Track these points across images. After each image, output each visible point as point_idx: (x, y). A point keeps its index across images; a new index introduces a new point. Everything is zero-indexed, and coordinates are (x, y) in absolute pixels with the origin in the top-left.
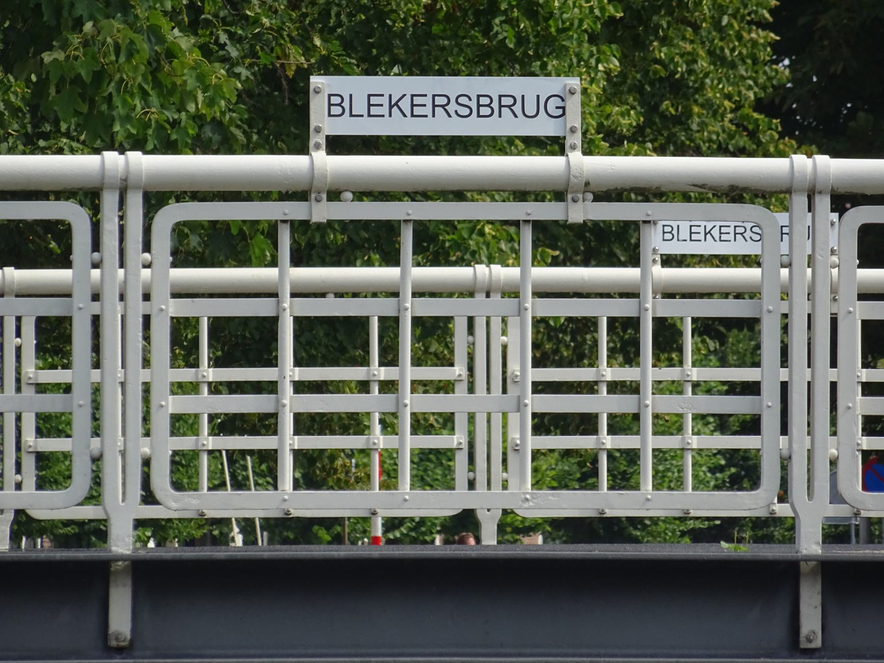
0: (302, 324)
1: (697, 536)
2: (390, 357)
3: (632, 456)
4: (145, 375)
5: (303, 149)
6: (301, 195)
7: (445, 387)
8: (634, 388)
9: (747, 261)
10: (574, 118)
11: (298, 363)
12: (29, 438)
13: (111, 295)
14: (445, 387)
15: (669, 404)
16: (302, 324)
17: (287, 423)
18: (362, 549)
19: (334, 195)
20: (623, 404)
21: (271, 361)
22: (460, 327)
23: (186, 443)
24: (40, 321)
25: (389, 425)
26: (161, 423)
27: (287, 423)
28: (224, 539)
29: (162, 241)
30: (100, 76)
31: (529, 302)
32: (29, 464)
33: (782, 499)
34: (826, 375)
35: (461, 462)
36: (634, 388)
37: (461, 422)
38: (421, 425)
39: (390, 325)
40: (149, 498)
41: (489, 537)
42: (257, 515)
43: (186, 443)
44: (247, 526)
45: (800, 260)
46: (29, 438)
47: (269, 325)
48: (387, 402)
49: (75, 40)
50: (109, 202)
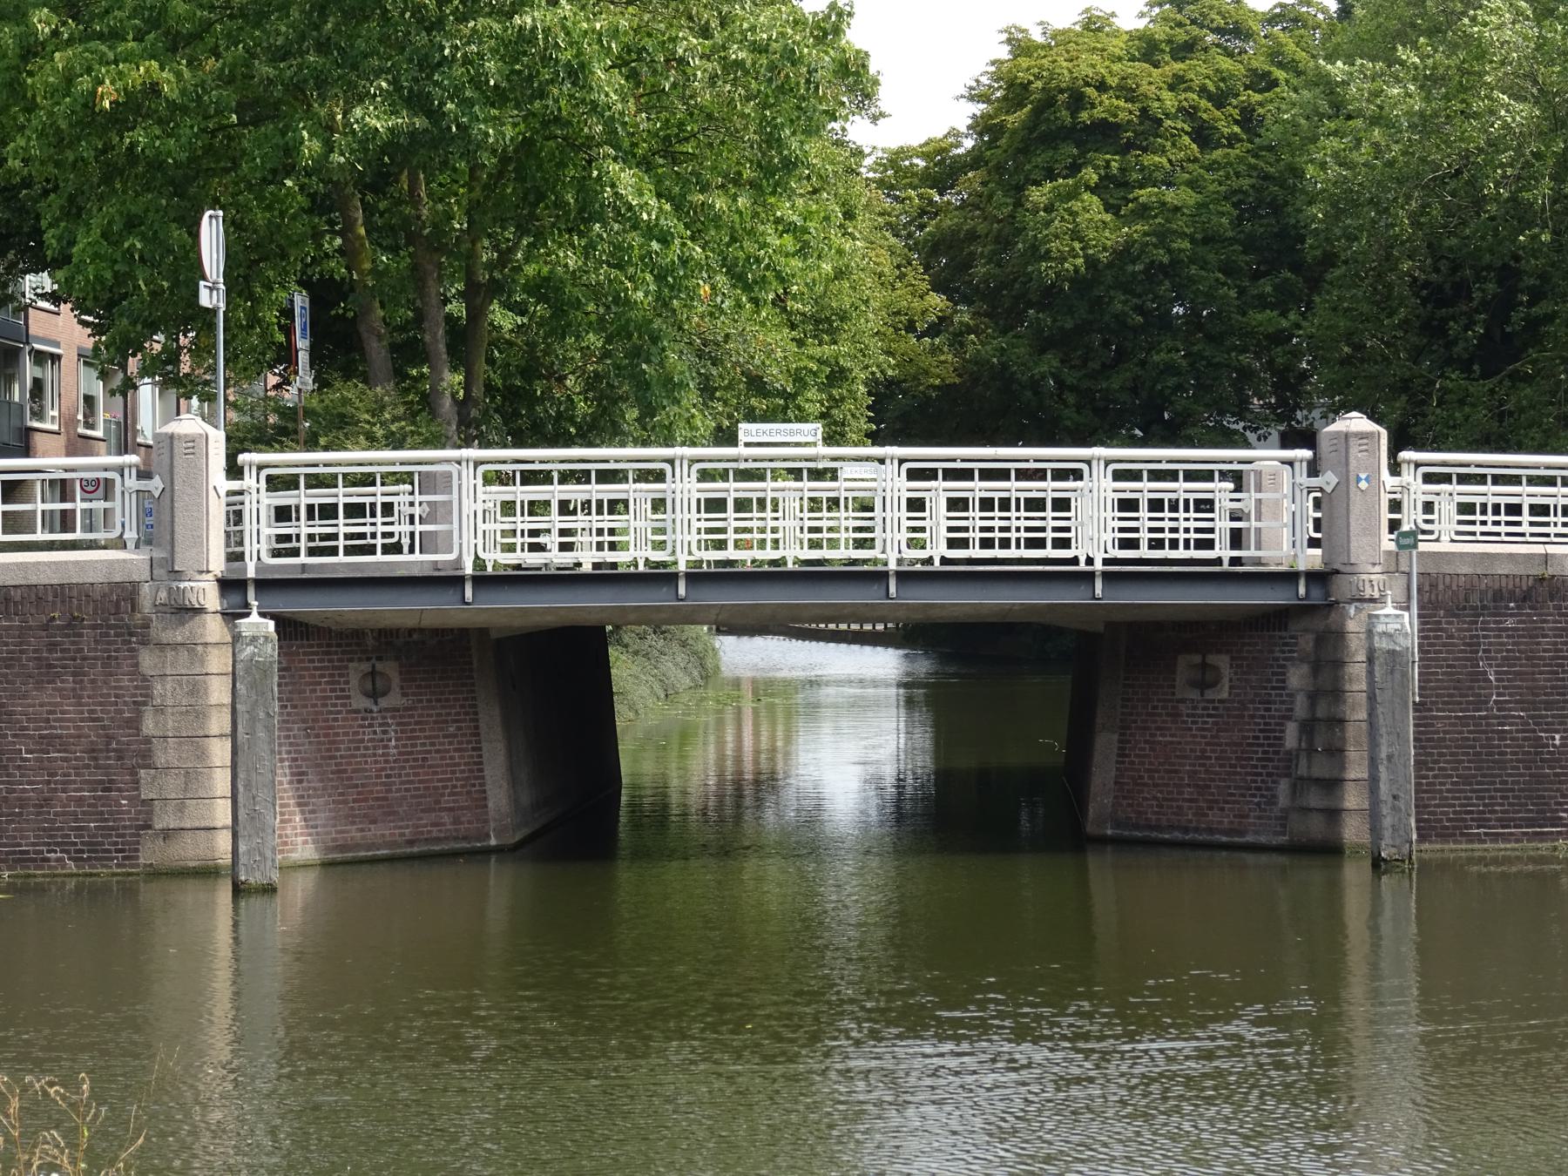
0: (1054, 500)
1: (845, 565)
2: (373, 515)
3: (764, 541)
4: (688, 516)
5: (736, 445)
6: (736, 460)
7: (392, 523)
8: (1176, 519)
9: (875, 480)
10: (820, 436)
11: (1044, 510)
12: (649, 536)
13: (678, 492)
14: (392, 523)
15: (1187, 524)
16: (1054, 500)
17: (341, 537)
18: (745, 569)
19: (746, 460)
20: (1173, 524)
21: (337, 518)
22: (396, 505)
23: (600, 539)
24: (653, 500)
25: (1018, 529)
26: (694, 531)
27: (341, 537)
28: (701, 567)
29: (694, 475)
30: (671, 424)
31: (1146, 493)
32: (649, 543)
33: (883, 552)
34: (687, 516)
35: (1073, 541)
36: (1176, 519)
37: (781, 530)
38: (811, 530)
39: (373, 505)
40: (690, 553)
41: (490, 569)
42: (712, 559)
43: (600, 539)
44: (709, 562)
45: (889, 480)
46: (649, 536)
47: (724, 501)
48: (372, 529)
49: (663, 413)
50: (677, 463)
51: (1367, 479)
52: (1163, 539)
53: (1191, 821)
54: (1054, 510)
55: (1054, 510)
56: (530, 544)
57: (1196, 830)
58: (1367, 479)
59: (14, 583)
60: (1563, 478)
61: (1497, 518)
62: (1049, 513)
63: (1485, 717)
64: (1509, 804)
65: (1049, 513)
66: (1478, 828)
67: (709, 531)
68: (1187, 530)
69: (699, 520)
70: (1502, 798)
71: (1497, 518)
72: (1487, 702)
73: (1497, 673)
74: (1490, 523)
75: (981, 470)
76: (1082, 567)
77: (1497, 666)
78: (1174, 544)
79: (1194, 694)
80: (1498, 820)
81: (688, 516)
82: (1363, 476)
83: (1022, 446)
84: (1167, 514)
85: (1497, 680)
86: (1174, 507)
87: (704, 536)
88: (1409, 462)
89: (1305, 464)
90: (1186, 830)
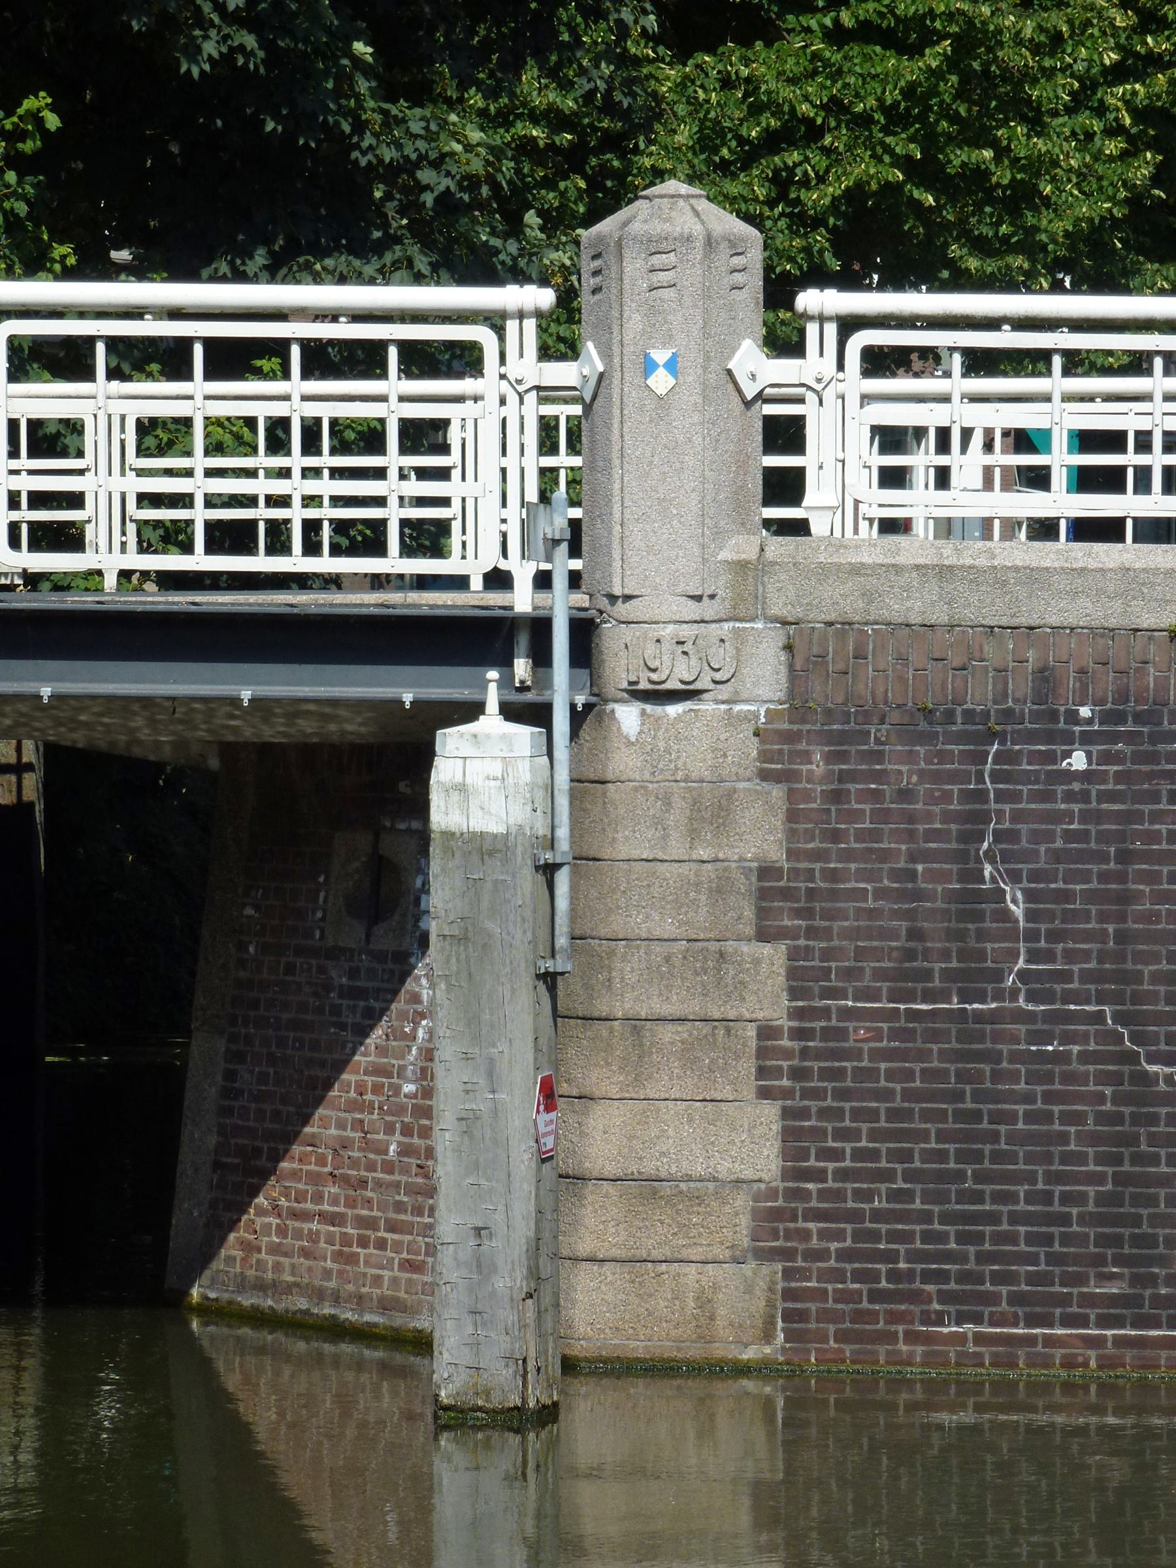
51: (671, 366)
52: (253, 523)
53: (327, 1274)
54: (404, 450)
55: (404, 450)
56: (34, 526)
57: (336, 1299)
58: (671, 366)
59: (1004, 621)
60: (1168, 356)
61: (312, 462)
62: (393, 458)
63: (993, 1017)
64: (1053, 1259)
65: (393, 458)
66: (960, 1320)
67: (39, 500)
68: (310, 501)
69: (943, 478)
70: (1030, 1239)
71: (312, 462)
72: (999, 976)
73: (1030, 896)
74: (296, 473)
75: (210, 344)
76: (476, 597)
77: (1035, 876)
78: (278, 541)
79: (352, 935)
80: (1017, 1299)
81: (504, 462)
82: (661, 356)
83: (881, 287)
84: (263, 460)
85: (1030, 915)
86: (278, 441)
87: (27, 515)
88: (822, 319)
89: (530, 325)
90: (320, 1295)
